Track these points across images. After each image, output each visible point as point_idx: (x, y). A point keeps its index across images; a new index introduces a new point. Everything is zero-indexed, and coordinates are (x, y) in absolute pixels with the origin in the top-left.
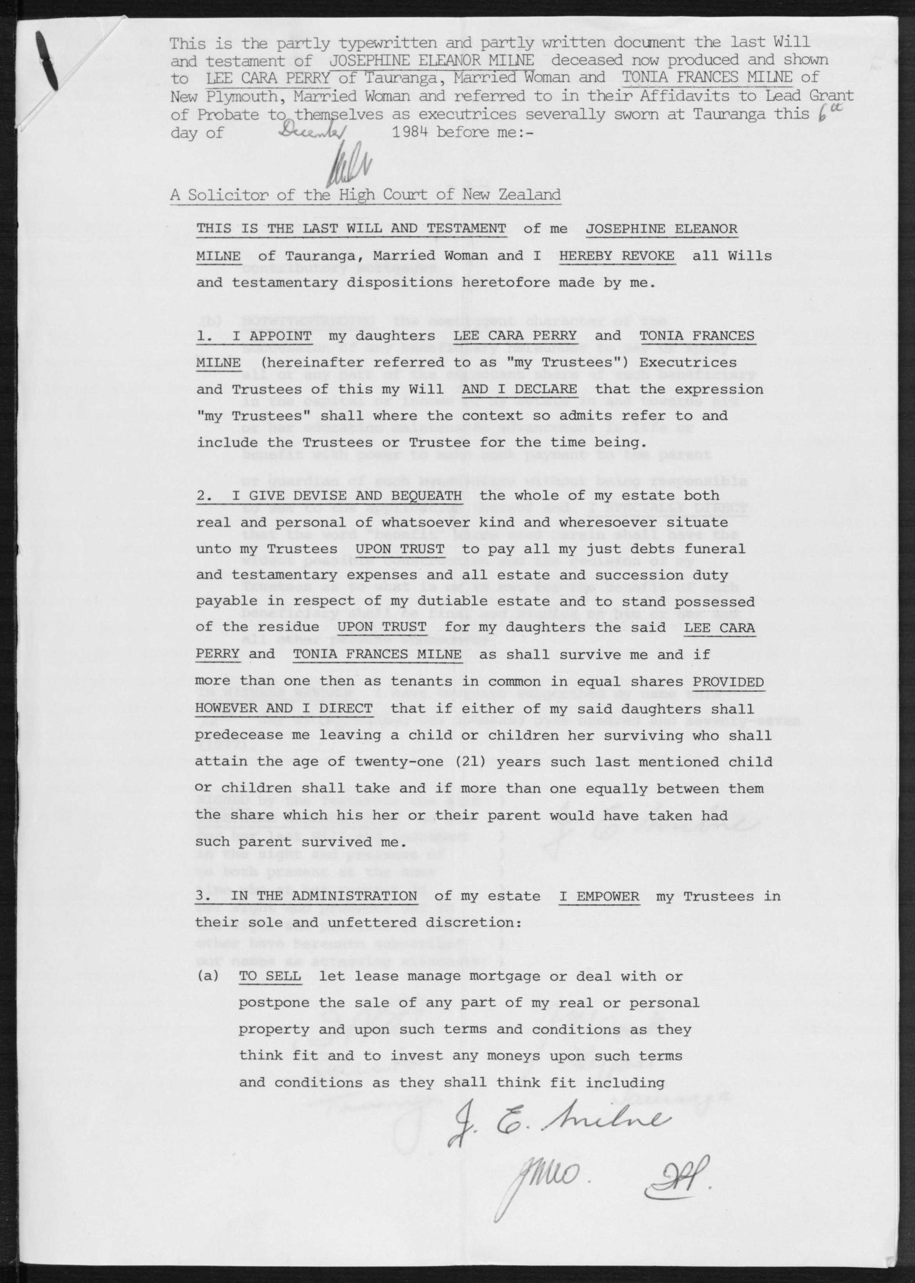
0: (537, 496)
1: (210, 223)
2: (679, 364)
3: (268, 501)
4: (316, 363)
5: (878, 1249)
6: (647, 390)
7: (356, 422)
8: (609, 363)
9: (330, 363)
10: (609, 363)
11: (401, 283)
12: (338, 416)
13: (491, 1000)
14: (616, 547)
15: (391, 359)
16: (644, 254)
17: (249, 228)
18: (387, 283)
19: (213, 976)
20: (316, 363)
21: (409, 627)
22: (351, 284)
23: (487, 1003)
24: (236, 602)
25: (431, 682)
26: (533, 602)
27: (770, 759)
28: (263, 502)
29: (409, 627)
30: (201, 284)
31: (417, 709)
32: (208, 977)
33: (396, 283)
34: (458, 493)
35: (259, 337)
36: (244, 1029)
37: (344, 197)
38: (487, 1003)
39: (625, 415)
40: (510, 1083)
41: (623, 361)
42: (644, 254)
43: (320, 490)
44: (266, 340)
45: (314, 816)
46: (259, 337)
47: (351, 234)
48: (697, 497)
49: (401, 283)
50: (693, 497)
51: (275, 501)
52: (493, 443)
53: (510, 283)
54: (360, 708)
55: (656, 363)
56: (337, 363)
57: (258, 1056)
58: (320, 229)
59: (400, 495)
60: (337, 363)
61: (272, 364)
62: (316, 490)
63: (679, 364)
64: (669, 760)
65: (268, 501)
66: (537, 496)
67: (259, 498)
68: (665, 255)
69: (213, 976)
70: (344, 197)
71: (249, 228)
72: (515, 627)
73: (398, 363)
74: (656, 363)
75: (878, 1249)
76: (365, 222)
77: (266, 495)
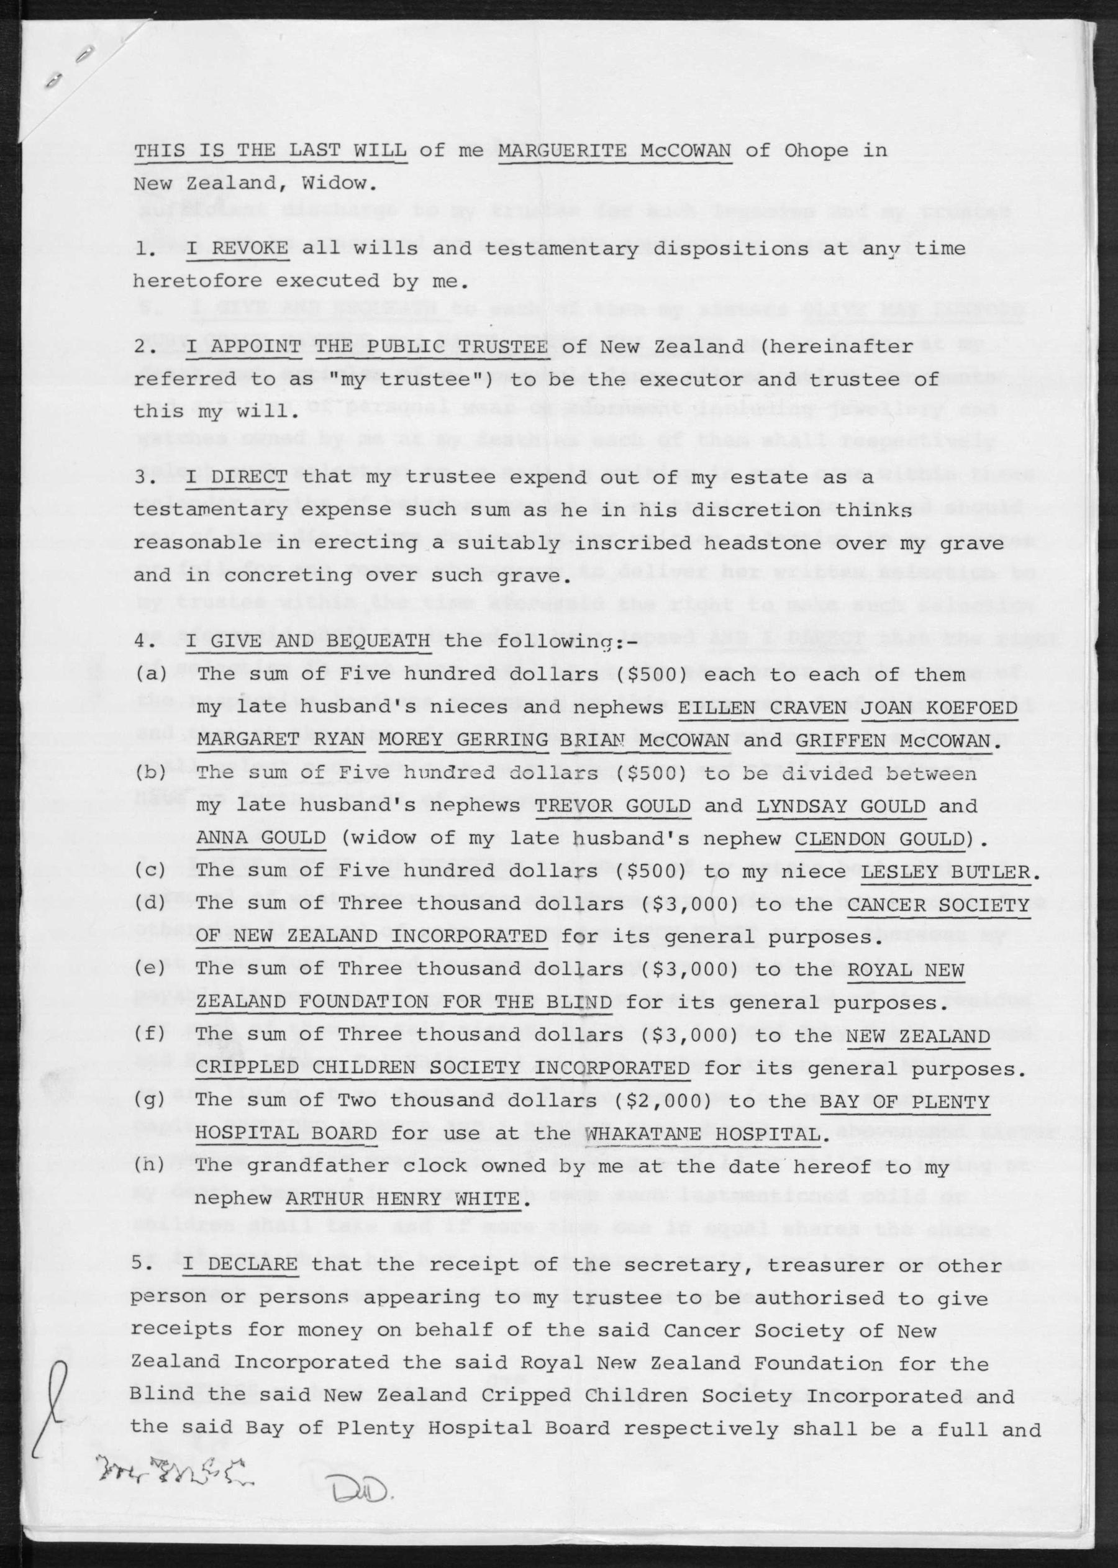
1: (153, 143)
2: (699, 382)
3: (238, 648)
7: (845, 1438)
9: (863, 348)
11: (733, 250)
14: (354, 1262)
16: (243, 245)
17: (210, 150)
21: (499, 347)
22: (698, 512)
24: (230, 544)
28: (230, 649)
29: (499, 347)
30: (140, 576)
33: (725, 250)
35: (224, 348)
37: (383, 1201)
39: (628, 1427)
40: (152, 412)
42: (243, 245)
44: (234, 352)
46: (224, 348)
47: (360, 158)
49: (733, 250)
51: (247, 649)
54: (270, 476)
55: (664, 381)
58: (316, 150)
59: (340, 640)
61: (776, 348)
63: (699, 382)
65: (238, 648)
67: (223, 642)
68: (275, 247)
70: (383, 1201)
71: (210, 150)
72: (742, 1166)
74: (301, 282)
76: (380, 141)
77: (235, 640)
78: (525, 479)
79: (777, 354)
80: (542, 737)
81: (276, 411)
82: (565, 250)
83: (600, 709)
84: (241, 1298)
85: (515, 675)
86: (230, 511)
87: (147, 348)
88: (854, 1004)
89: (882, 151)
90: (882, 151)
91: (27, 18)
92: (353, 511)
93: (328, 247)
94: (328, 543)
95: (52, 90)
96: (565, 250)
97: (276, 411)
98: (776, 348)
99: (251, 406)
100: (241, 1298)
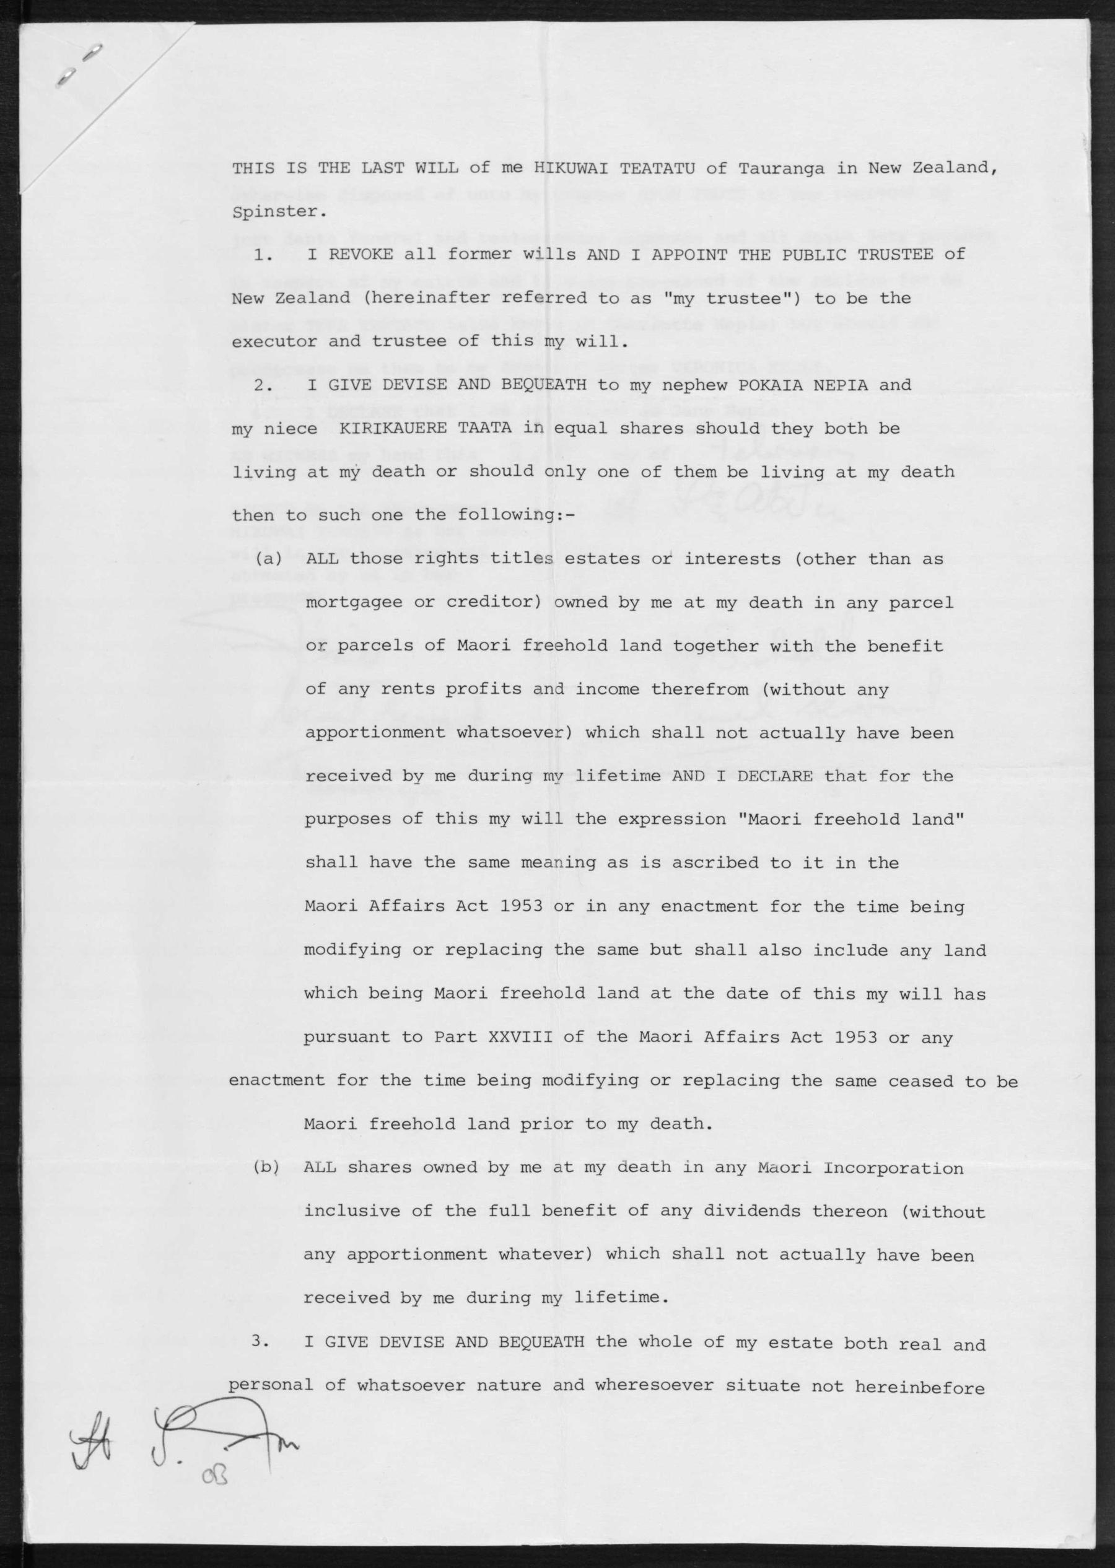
0: (581, 647)
4: (431, 299)
5: (1078, 1531)
6: (606, 1037)
8: (775, 300)
9: (448, 299)
10: (775, 300)
12: (381, 862)
13: (470, 1035)
14: (318, 1078)
15: (523, 293)
18: (354, 820)
19: (275, 559)
20: (431, 299)
22: (709, 1212)
23: (466, 1038)
25: (374, 1038)
26: (390, 1386)
27: (897, 816)
31: (318, 473)
32: (269, 560)
34: (581, 382)
36: (452, 690)
38: (466, 1038)
40: (829, 994)
41: (794, 297)
42: (356, 252)
43: (416, 377)
45: (342, 994)
48: (841, 430)
50: (836, 430)
52: (895, 777)
53: (517, 603)
55: (252, 343)
56: (457, 298)
57: (836, 995)
60: (457, 298)
61: (377, 299)
62: (410, 377)
63: (280, 343)
64: (817, 557)
66: (581, 647)
69: (275, 559)
73: (532, 298)
74: (252, 343)
75: (1078, 1531)
78: (244, 343)
79: (377, 304)
80: (385, 1344)
81: (609, 341)
82: (458, 1255)
83: (684, 387)
84: (570, 908)
85: (906, 473)
86: (408, 689)
87: (265, 387)
88: (322, 820)
89: (699, 1168)
90: (699, 1168)
91: (29, 20)
92: (737, 908)
93: (694, 732)
94: (845, 1213)
95: (63, 87)
96: (458, 1255)
97: (609, 341)
98: (377, 299)
99: (783, 642)
100: (570, 908)
